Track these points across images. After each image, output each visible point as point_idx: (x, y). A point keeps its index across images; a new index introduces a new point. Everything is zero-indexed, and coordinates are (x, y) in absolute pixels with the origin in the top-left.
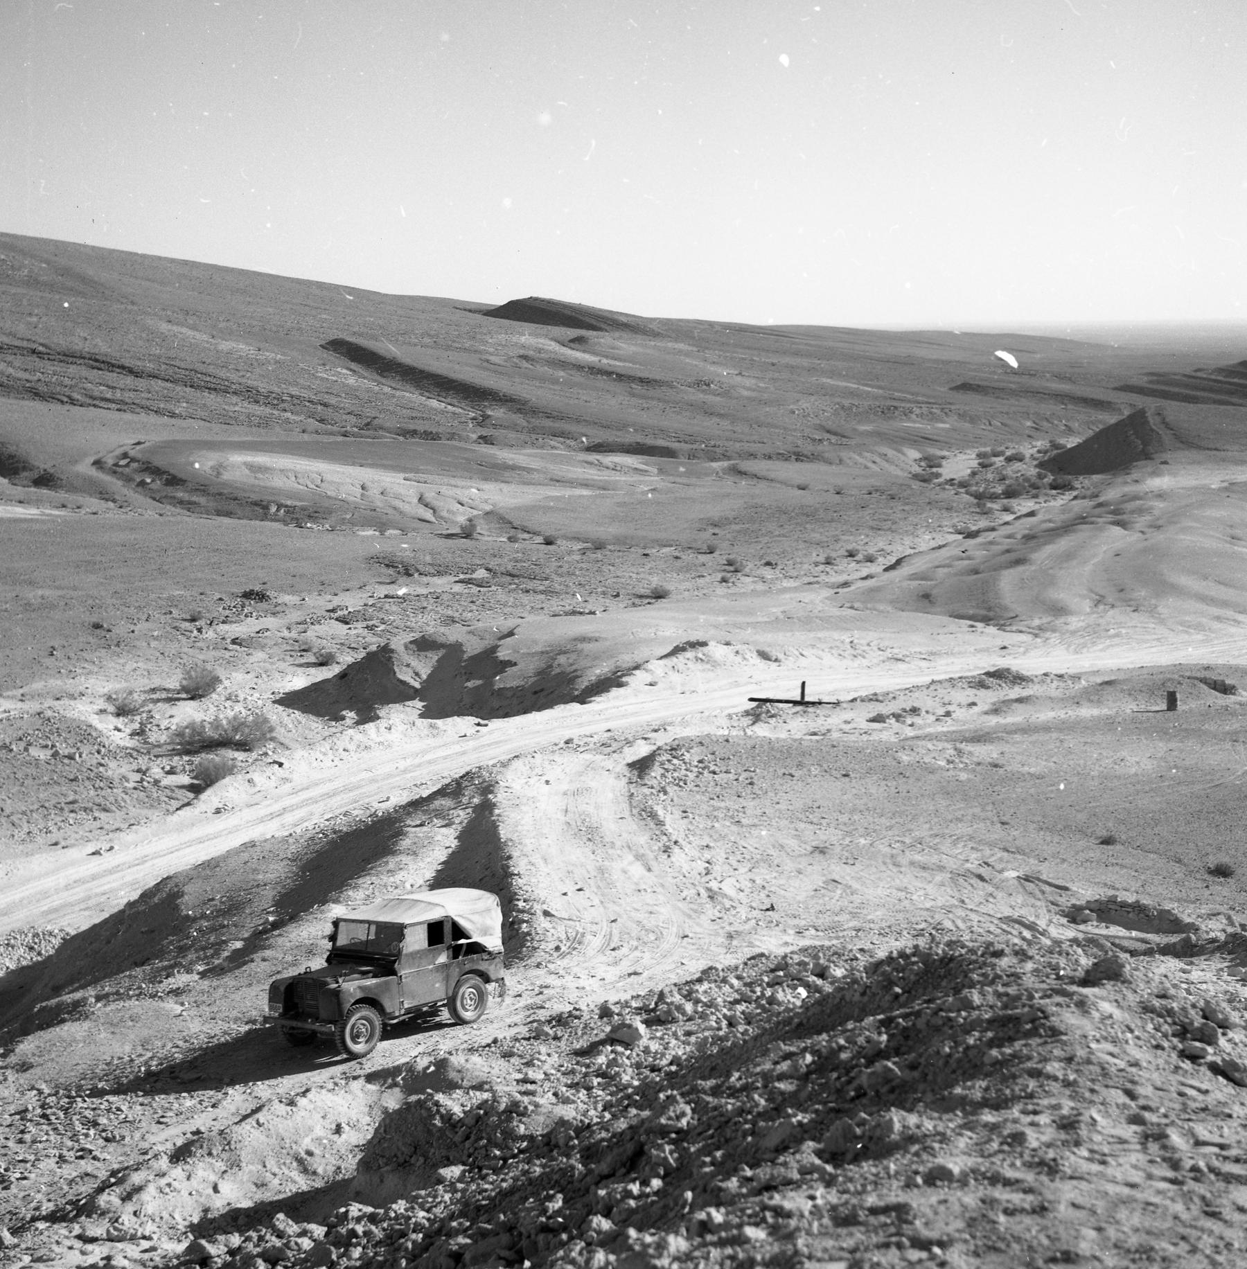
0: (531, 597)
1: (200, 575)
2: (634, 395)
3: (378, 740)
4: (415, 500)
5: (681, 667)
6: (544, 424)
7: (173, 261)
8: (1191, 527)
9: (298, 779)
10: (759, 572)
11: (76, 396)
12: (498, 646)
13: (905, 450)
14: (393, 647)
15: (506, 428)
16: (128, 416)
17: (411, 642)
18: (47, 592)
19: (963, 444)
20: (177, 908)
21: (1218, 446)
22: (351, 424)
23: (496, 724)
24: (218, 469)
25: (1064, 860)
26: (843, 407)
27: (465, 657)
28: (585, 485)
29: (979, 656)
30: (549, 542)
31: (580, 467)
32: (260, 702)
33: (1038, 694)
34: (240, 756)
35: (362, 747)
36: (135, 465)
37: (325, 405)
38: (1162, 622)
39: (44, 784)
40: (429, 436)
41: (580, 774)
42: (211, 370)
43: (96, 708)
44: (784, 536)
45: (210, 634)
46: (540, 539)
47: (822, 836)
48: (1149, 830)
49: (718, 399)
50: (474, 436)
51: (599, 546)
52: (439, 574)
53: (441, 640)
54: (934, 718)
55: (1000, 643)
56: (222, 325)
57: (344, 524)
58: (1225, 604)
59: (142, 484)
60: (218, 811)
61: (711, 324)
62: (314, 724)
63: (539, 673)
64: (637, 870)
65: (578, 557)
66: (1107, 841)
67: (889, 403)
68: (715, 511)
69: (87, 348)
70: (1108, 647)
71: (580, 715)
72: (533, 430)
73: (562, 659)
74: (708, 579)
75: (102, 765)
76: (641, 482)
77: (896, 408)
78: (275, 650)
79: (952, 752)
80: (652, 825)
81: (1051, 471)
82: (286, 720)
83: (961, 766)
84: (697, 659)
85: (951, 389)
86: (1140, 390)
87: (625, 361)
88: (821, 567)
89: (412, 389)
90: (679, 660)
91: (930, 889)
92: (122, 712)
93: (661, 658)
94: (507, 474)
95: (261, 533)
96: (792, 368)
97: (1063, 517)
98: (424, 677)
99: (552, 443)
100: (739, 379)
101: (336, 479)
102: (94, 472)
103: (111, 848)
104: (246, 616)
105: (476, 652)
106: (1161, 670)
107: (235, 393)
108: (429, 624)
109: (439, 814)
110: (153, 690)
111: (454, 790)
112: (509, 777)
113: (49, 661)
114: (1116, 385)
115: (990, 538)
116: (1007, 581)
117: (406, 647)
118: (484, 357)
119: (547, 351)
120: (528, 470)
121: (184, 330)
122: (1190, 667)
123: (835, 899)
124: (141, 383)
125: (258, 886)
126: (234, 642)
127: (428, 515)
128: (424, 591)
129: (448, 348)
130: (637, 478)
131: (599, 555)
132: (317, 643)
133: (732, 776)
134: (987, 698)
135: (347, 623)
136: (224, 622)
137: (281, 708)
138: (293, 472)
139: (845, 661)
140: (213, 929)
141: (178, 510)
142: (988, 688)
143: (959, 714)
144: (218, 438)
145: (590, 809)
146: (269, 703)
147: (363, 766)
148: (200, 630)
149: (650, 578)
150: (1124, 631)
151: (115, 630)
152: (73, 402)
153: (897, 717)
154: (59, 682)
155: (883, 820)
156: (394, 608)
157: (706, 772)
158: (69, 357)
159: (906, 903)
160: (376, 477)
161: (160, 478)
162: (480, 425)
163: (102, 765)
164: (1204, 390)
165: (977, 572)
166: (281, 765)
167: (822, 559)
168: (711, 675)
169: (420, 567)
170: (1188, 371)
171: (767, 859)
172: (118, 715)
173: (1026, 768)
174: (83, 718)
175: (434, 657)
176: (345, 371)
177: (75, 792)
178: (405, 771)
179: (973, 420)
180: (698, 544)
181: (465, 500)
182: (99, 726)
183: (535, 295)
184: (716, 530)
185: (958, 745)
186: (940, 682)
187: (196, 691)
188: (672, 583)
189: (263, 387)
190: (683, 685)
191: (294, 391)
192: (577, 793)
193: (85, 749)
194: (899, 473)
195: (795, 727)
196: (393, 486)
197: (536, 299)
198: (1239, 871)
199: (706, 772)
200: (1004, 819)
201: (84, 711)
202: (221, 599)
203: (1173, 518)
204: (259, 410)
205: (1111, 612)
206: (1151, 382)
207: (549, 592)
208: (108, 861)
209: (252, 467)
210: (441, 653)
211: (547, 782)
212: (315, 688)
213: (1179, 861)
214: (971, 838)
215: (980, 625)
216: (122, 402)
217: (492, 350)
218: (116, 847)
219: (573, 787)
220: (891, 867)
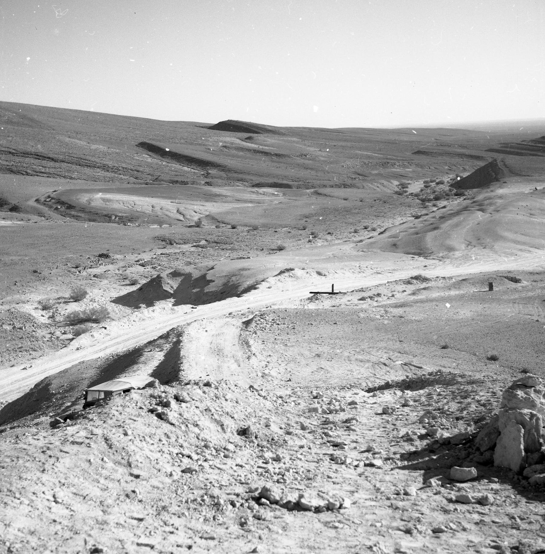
0: (224, 252)
1: (80, 248)
2: (273, 162)
3: (148, 316)
4: (175, 211)
5: (282, 280)
6: (233, 176)
7: (71, 110)
8: (512, 211)
9: (113, 334)
10: (325, 237)
11: (29, 171)
12: (207, 274)
13: (392, 181)
14: (162, 276)
15: (217, 178)
16: (51, 179)
17: (170, 274)
18: (14, 258)
19: (417, 178)
20: (48, 390)
21: (529, 174)
22: (149, 179)
23: (200, 307)
24: (89, 201)
25: (424, 356)
26: (365, 163)
27: (193, 279)
28: (251, 202)
29: (414, 270)
30: (234, 227)
31: (249, 194)
32: (105, 302)
33: (433, 286)
34: (95, 325)
35: (142, 319)
36: (53, 201)
37: (138, 171)
38: (496, 252)
39: (9, 340)
40: (184, 183)
41: (222, 327)
42: (88, 157)
43: (34, 307)
44: (336, 221)
45: (84, 273)
46: (230, 226)
47: (320, 349)
48: (463, 342)
49: (311, 162)
50: (203, 182)
51: (255, 228)
52: (185, 243)
53: (183, 272)
54: (387, 298)
55: (424, 264)
56: (92, 138)
57: (144, 223)
58: (524, 244)
59: (57, 209)
60: (78, 349)
61: (310, 129)
62: (127, 310)
63: (224, 285)
64: (234, 366)
65: (246, 234)
66: (444, 347)
67: (385, 161)
68: (306, 211)
69: (33, 150)
70: (471, 264)
71: (237, 302)
72: (229, 179)
73: (234, 278)
74: (303, 241)
75: (34, 331)
76: (275, 200)
77: (388, 163)
78: (112, 279)
79: (383, 312)
80: (246, 347)
81: (455, 188)
82: (116, 309)
83: (387, 318)
84: (290, 276)
85: (412, 154)
86: (497, 151)
87: (269, 146)
88: (352, 234)
89: (176, 163)
90: (283, 275)
91: (362, 370)
92: (45, 308)
93: (276, 276)
94: (216, 198)
95: (107, 228)
96: (343, 147)
97: (458, 208)
98: (175, 288)
99: (238, 184)
100: (320, 152)
101: (140, 203)
102: (35, 205)
103: (31, 366)
104: (100, 265)
105: (197, 277)
106: (489, 273)
107: (98, 167)
108: (180, 265)
109: (159, 346)
110: (59, 298)
111: (165, 337)
112: (189, 330)
113: (14, 288)
114: (486, 149)
115: (425, 219)
116: (430, 238)
117: (167, 276)
118: (207, 147)
119: (235, 144)
120: (226, 196)
121: (76, 141)
122: (502, 272)
123: (321, 375)
124: (57, 165)
125: (82, 379)
126: (94, 276)
127: (181, 218)
128: (178, 251)
129: (191, 144)
130: (274, 198)
131: (255, 232)
132: (130, 276)
133: (286, 326)
134: (410, 288)
135: (144, 266)
136: (90, 268)
137: (113, 304)
138: (121, 201)
139: (355, 275)
140: (62, 398)
141: (72, 220)
142: (412, 284)
143: (398, 295)
144: (90, 188)
145: (222, 342)
146: (109, 303)
147: (141, 328)
148: (80, 272)
149: (277, 241)
150: (479, 257)
151: (43, 273)
152: (27, 174)
153: (371, 298)
154: (18, 296)
155: (349, 342)
156: (165, 259)
157: (275, 324)
158: (26, 154)
159: (350, 376)
160: (158, 202)
161: (64, 206)
162: (206, 177)
163: (34, 331)
164: (525, 149)
165: (417, 234)
166: (105, 328)
167: (353, 230)
168: (296, 283)
169: (176, 240)
170: (519, 142)
171: (294, 360)
172: (43, 310)
173: (414, 318)
174: (28, 312)
175: (179, 279)
176: (146, 156)
177: (22, 343)
178: (159, 329)
179: (422, 167)
180: (299, 226)
181: (197, 210)
182: (34, 315)
183: (230, 119)
184: (307, 220)
185: (387, 309)
186: (391, 282)
187: (77, 298)
188: (287, 243)
189: (110, 164)
190: (282, 287)
191: (124, 165)
192: (218, 335)
193: (27, 325)
194: (389, 191)
195: (326, 303)
196: (166, 205)
197: (231, 121)
198: (501, 358)
199: (275, 324)
200: (401, 339)
201: (28, 309)
202: (89, 258)
203: (505, 207)
204: (109, 174)
205: (474, 249)
206: (502, 147)
207: (232, 249)
208: (29, 372)
209: (103, 200)
210: (182, 278)
211: (206, 331)
212: (129, 294)
213: (475, 355)
214: (385, 348)
215: (416, 257)
216: (50, 173)
217: (211, 144)
218: (33, 366)
219: (217, 333)
220: (347, 361)
